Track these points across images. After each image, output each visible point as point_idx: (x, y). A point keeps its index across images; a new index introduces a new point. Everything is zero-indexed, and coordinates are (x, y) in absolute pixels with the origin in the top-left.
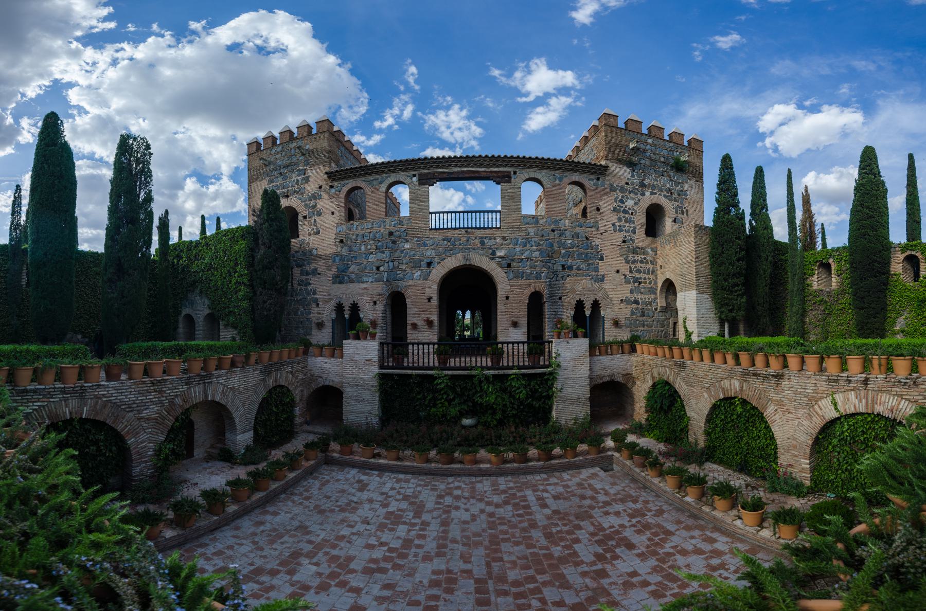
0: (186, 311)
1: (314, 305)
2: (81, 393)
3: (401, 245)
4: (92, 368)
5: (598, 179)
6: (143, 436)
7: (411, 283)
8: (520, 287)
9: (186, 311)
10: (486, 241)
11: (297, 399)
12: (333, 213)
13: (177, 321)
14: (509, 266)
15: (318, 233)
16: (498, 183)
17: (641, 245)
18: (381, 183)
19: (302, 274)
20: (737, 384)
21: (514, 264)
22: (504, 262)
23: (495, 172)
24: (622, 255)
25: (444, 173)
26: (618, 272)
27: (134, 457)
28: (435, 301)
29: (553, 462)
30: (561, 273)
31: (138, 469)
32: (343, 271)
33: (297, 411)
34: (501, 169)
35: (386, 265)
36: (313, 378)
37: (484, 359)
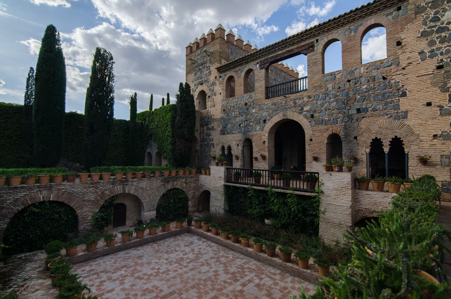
0: (148, 150)
1: (212, 147)
2: (50, 188)
4: (57, 176)
6: (85, 209)
7: (255, 133)
8: (320, 131)
9: (148, 150)
10: (297, 101)
11: (190, 197)
13: (144, 156)
14: (312, 116)
15: (214, 106)
16: (306, 55)
19: (207, 130)
20: (378, 256)
21: (316, 115)
22: (309, 115)
27: (80, 220)
28: (267, 144)
29: (289, 264)
31: (82, 227)
32: (225, 128)
33: (190, 203)
35: (244, 123)
36: (201, 186)
37: (298, 183)
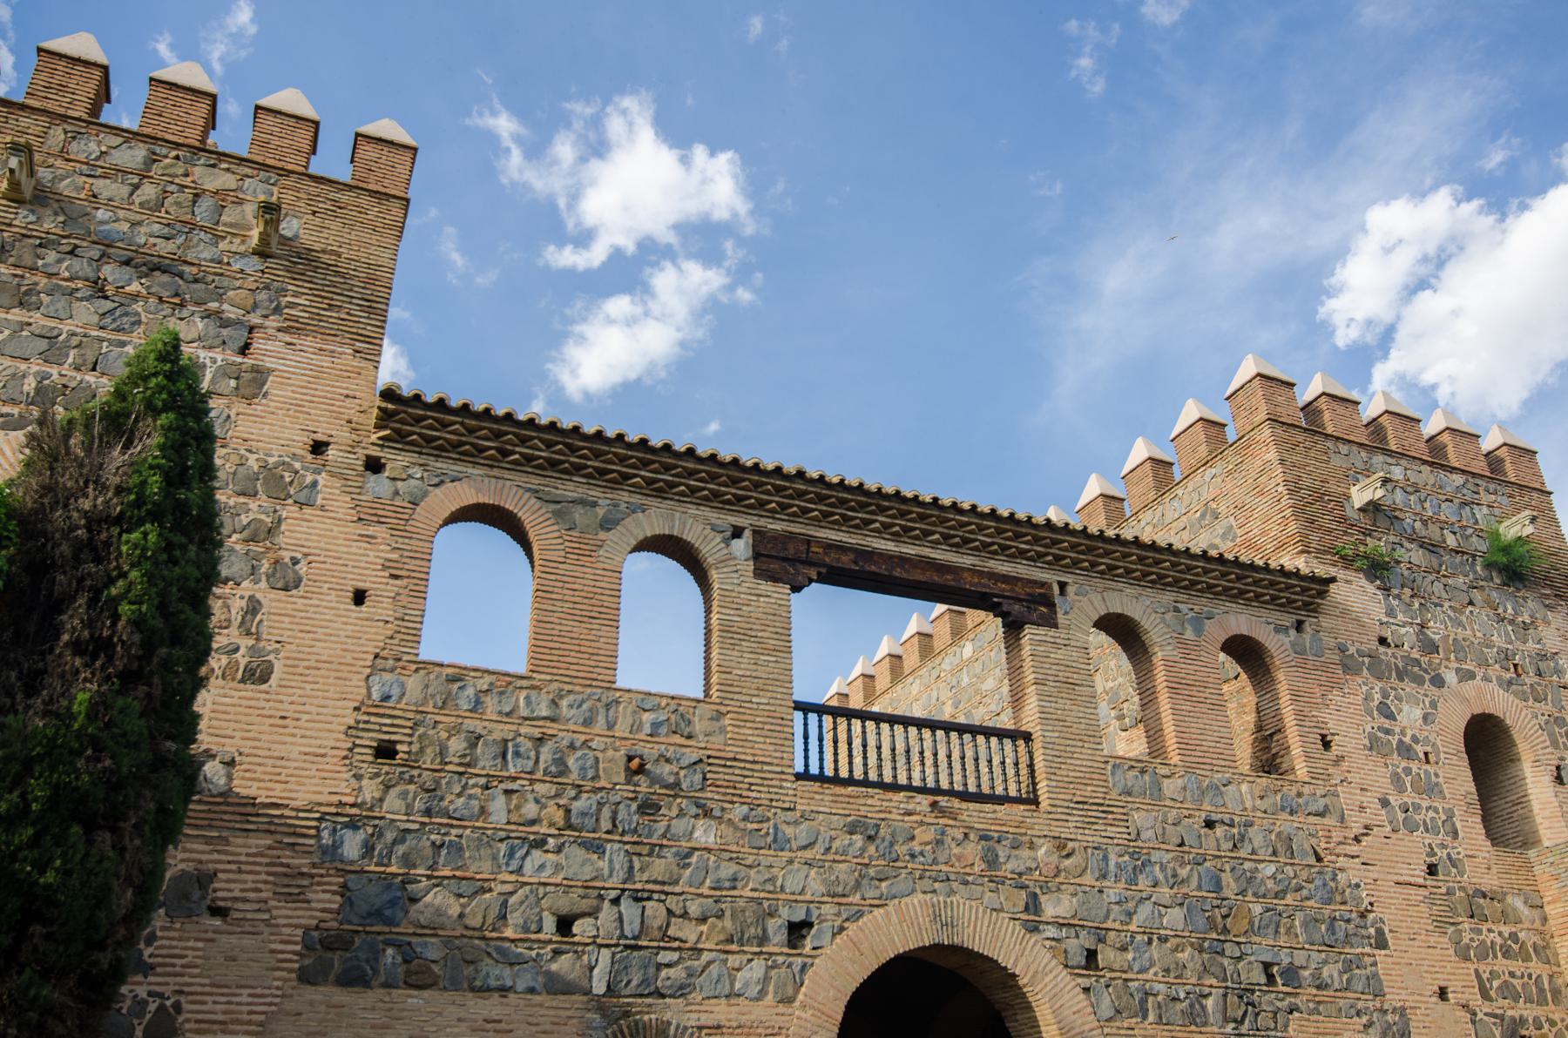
3: (679, 826)
5: (1299, 626)
12: (359, 597)
17: (1489, 882)
18: (607, 524)
21: (1106, 956)
22: (1076, 945)
23: (1005, 578)
24: (1440, 924)
25: (841, 548)
26: (1442, 994)
30: (1266, 1001)
34: (1022, 570)
35: (607, 913)
